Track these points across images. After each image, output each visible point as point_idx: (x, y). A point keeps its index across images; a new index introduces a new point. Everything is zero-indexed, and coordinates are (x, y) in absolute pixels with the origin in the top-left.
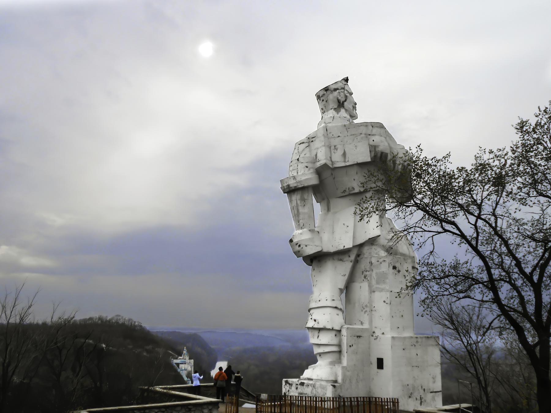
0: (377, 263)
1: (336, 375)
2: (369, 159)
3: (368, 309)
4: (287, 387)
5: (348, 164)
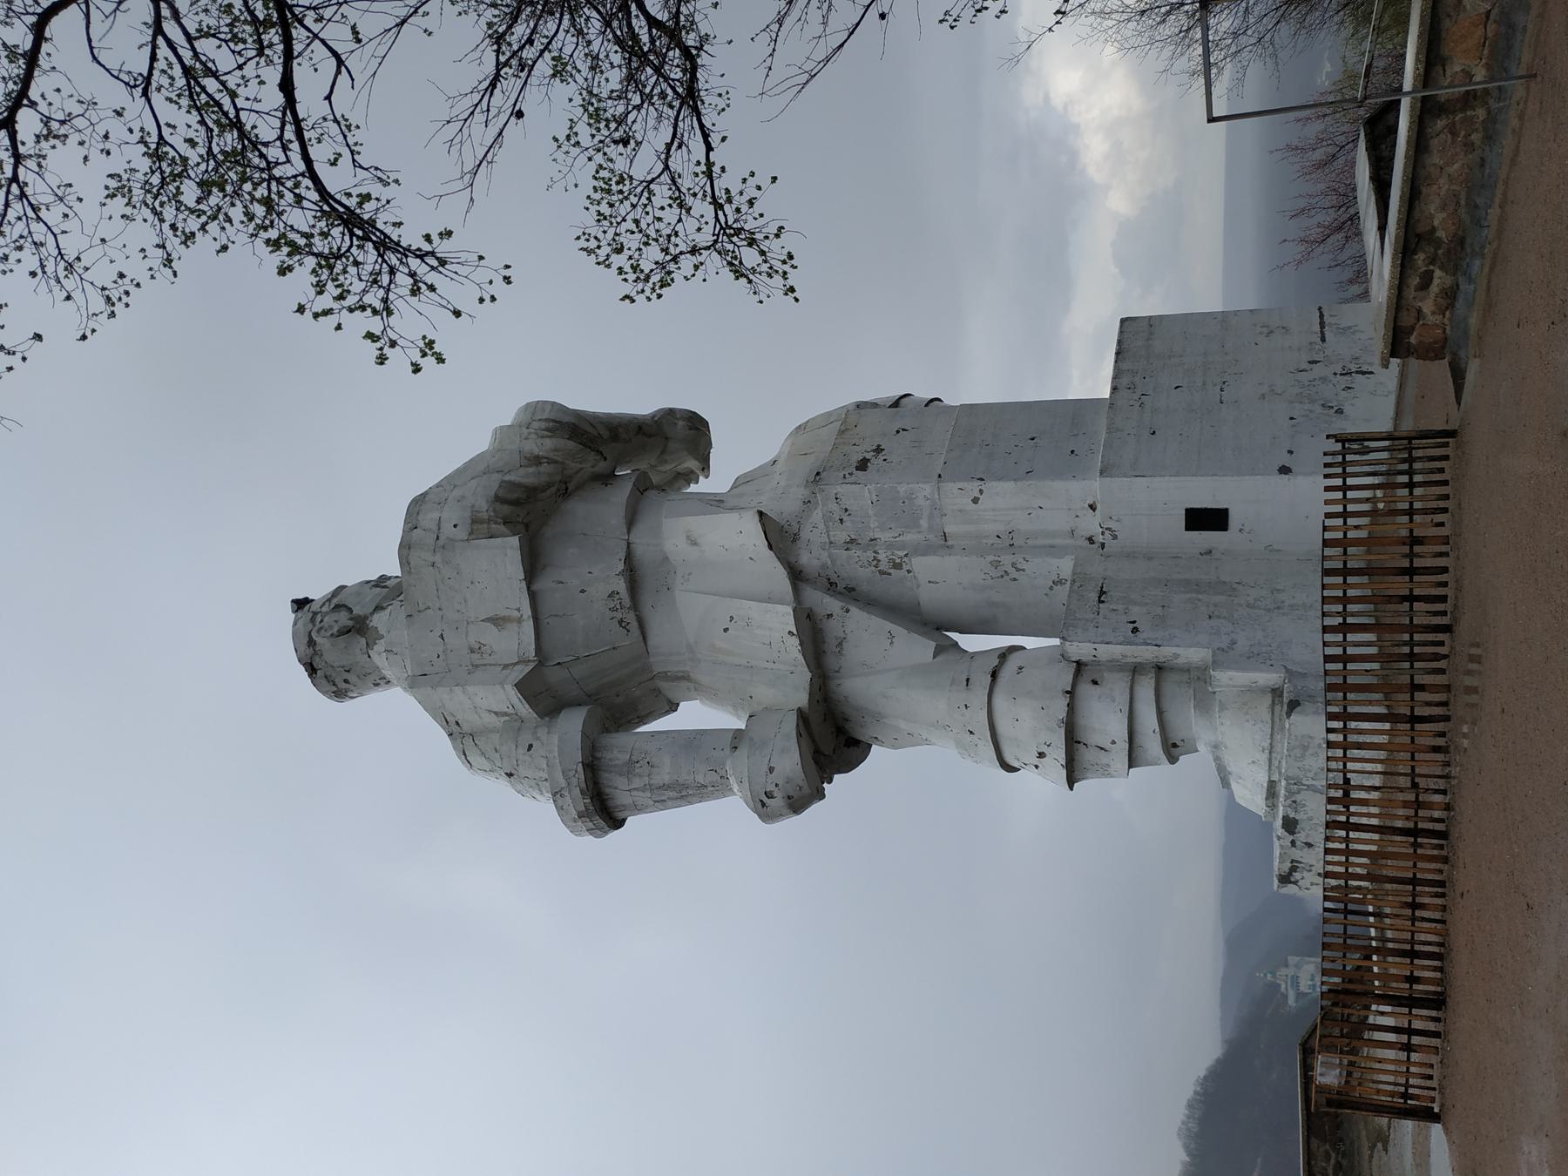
0: (847, 524)
1: (1252, 690)
2: (514, 541)
3: (1007, 560)
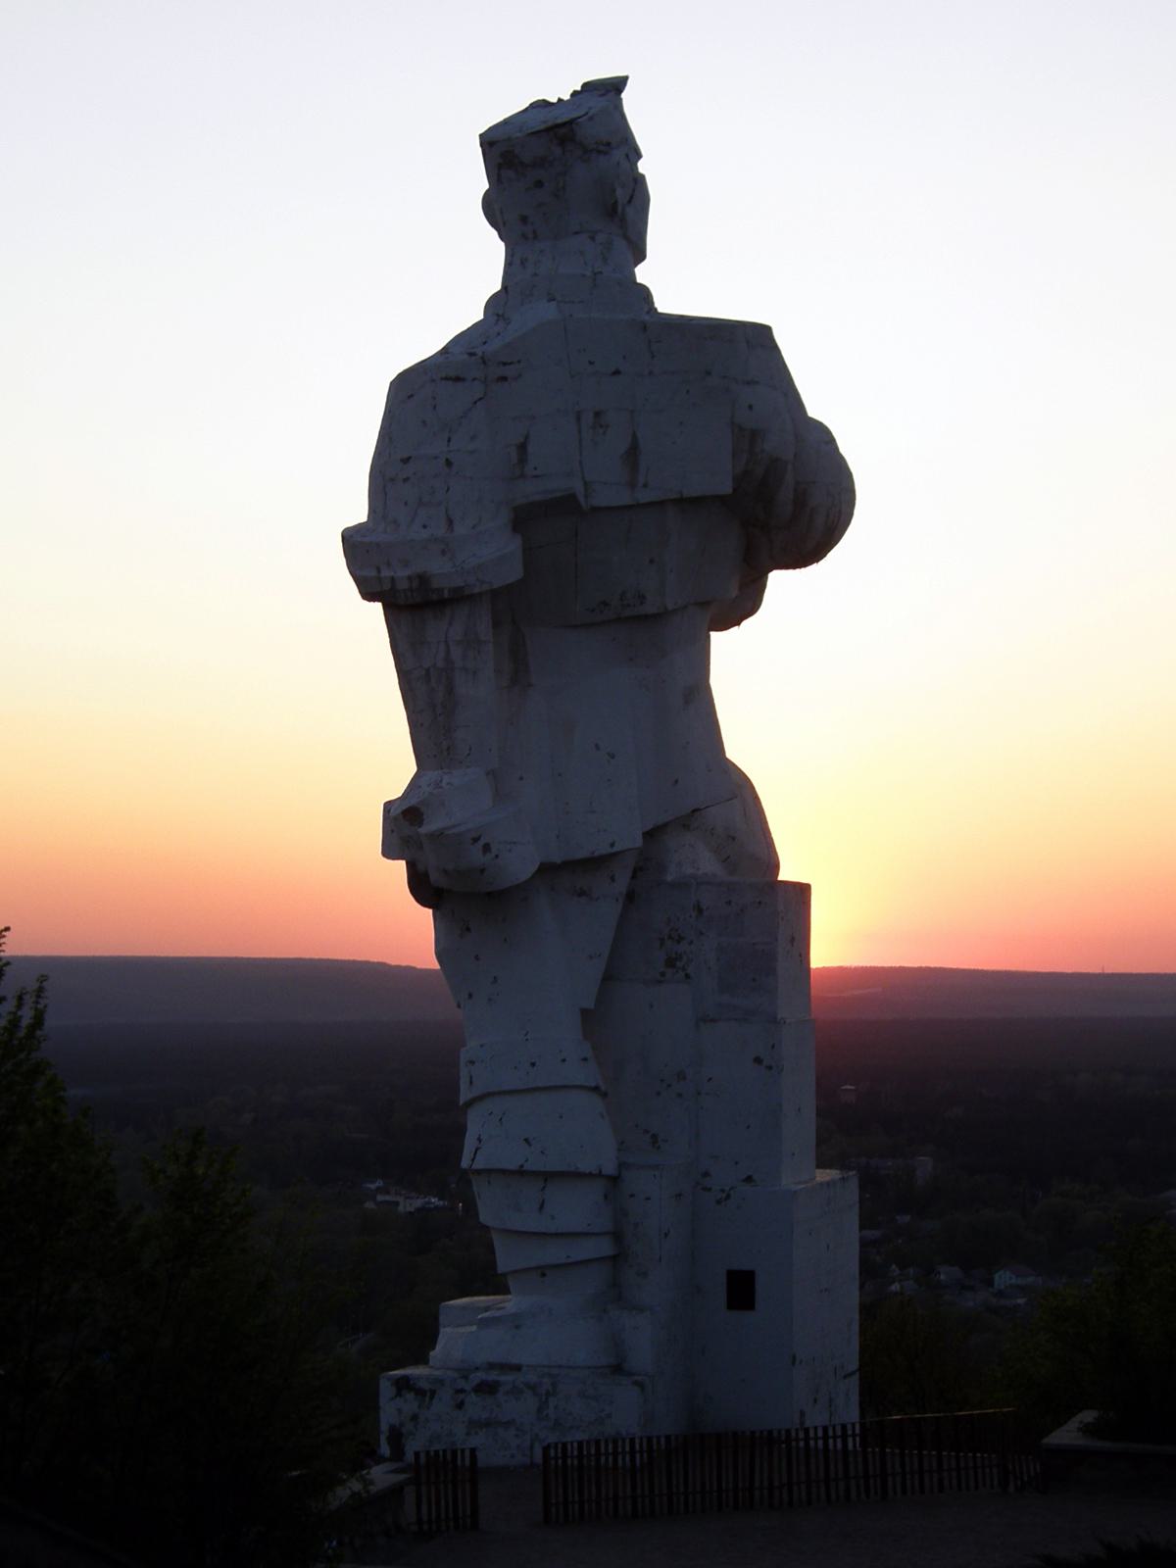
4: (410, 1403)
5: (644, 497)
